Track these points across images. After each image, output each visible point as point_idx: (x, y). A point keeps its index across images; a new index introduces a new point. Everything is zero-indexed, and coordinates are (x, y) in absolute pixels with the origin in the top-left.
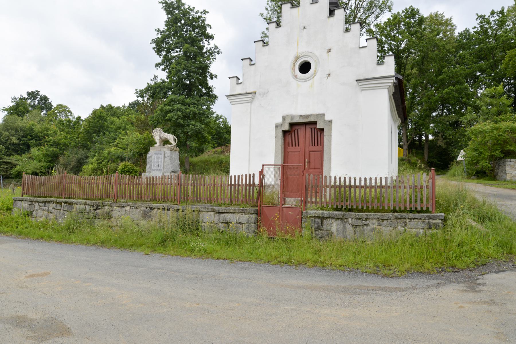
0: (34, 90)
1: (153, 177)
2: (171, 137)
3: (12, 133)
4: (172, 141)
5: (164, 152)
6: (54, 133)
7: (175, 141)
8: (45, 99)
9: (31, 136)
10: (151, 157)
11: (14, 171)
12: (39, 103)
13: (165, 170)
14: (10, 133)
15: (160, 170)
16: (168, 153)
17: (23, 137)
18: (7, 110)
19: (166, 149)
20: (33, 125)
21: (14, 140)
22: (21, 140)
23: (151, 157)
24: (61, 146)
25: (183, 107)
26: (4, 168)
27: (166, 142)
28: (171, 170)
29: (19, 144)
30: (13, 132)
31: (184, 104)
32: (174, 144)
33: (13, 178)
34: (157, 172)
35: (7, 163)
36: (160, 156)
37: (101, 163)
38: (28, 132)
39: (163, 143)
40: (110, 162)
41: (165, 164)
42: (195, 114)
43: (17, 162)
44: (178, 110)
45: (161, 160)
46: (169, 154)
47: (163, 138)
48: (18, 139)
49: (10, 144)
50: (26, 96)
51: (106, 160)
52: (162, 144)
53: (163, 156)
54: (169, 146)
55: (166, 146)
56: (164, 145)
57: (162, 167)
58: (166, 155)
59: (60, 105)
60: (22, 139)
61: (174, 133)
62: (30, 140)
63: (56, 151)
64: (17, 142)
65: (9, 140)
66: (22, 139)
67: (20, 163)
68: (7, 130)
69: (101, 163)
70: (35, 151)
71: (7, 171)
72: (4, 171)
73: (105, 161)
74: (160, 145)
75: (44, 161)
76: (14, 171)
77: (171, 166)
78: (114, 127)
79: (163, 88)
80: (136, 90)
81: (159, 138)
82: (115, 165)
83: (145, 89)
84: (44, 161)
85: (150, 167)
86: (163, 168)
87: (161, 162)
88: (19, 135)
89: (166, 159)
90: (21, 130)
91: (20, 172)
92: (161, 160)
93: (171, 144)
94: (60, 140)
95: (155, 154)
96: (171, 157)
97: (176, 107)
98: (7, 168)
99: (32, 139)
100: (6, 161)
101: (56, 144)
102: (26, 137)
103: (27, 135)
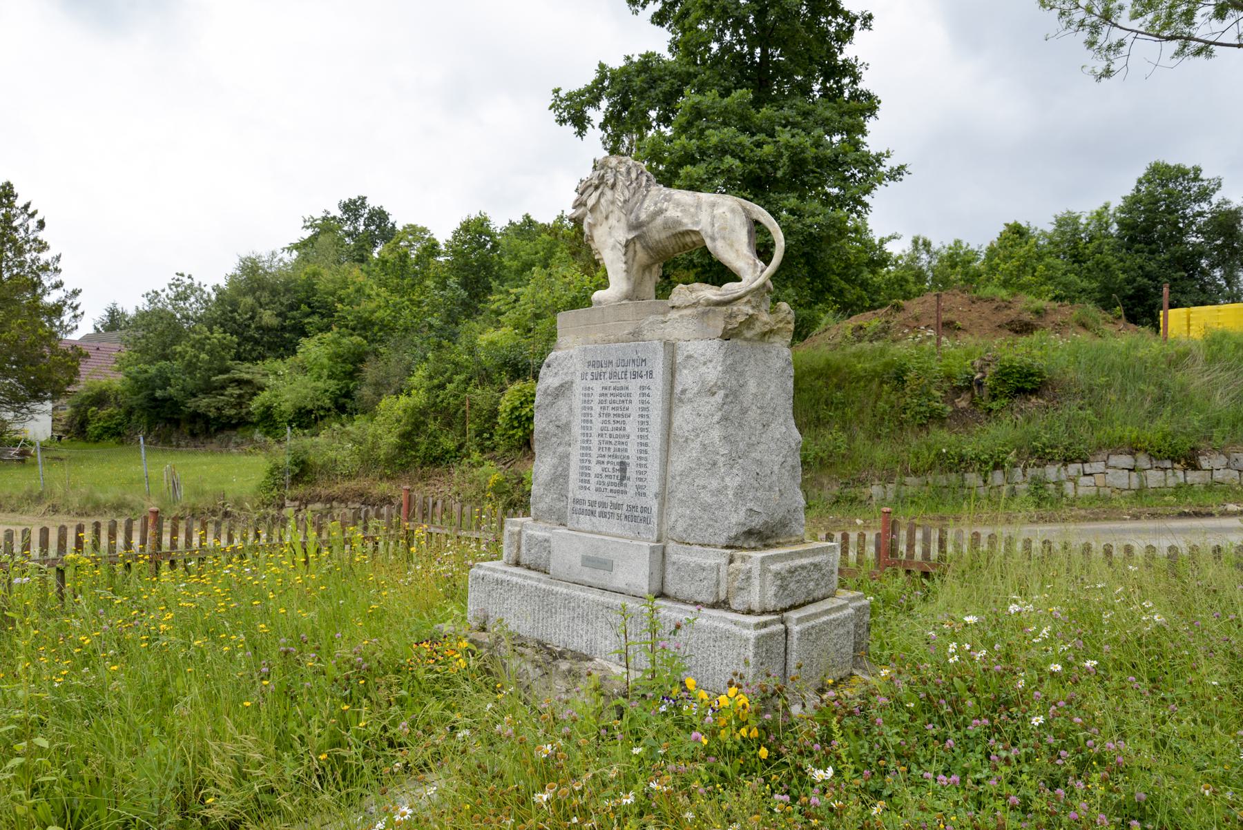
0: (354, 197)
1: (626, 450)
2: (720, 219)
3: (262, 300)
4: (735, 251)
5: (670, 348)
6: (358, 291)
7: (763, 251)
8: (379, 216)
9: (309, 305)
10: (563, 390)
11: (255, 404)
12: (367, 226)
13: (678, 517)
14: (258, 300)
15: (636, 516)
16: (704, 356)
17: (292, 307)
18: (296, 247)
19: (685, 322)
20: (315, 274)
21: (268, 317)
22: (286, 318)
23: (563, 390)
24: (376, 328)
25: (745, 139)
26: (231, 395)
27: (683, 262)
28: (735, 519)
29: (283, 329)
30: (265, 297)
31: (746, 127)
32: (753, 274)
33: (256, 425)
34: (614, 526)
35: (240, 383)
36: (634, 385)
37: (442, 386)
38: (302, 295)
39: (654, 277)
40: (475, 381)
41: (679, 463)
42: (798, 163)
43: (264, 380)
44: (722, 150)
45: (644, 427)
46: (713, 373)
47: (657, 233)
48: (278, 315)
49: (258, 328)
50: (338, 213)
51: (462, 377)
52: (649, 286)
53: (657, 385)
54: (709, 293)
55: (681, 294)
56: (664, 290)
57: (653, 486)
58: (686, 378)
59: (411, 226)
60: (290, 314)
61: (755, 184)
62: (308, 315)
63: (360, 345)
64: (275, 322)
65: (257, 319)
66: (290, 314)
67: (271, 380)
68: (252, 291)
69: (442, 386)
70: (313, 349)
71: (240, 405)
72: (233, 406)
73: (457, 378)
74: (633, 295)
75: (329, 377)
76: (255, 404)
77: (732, 482)
78: (515, 264)
79: (661, 79)
80: (557, 91)
81: (622, 235)
82: (489, 391)
83: (589, 90)
84: (329, 377)
85: (559, 478)
86: (663, 496)
87: (641, 437)
88: (282, 304)
89: (684, 418)
90: (288, 290)
91: (269, 408)
92: (644, 427)
93: (719, 273)
94: (373, 312)
95: (597, 367)
96: (733, 395)
97: (714, 137)
98: (240, 396)
99: (313, 313)
100: (236, 376)
101: (364, 325)
102: (298, 308)
103: (301, 301)
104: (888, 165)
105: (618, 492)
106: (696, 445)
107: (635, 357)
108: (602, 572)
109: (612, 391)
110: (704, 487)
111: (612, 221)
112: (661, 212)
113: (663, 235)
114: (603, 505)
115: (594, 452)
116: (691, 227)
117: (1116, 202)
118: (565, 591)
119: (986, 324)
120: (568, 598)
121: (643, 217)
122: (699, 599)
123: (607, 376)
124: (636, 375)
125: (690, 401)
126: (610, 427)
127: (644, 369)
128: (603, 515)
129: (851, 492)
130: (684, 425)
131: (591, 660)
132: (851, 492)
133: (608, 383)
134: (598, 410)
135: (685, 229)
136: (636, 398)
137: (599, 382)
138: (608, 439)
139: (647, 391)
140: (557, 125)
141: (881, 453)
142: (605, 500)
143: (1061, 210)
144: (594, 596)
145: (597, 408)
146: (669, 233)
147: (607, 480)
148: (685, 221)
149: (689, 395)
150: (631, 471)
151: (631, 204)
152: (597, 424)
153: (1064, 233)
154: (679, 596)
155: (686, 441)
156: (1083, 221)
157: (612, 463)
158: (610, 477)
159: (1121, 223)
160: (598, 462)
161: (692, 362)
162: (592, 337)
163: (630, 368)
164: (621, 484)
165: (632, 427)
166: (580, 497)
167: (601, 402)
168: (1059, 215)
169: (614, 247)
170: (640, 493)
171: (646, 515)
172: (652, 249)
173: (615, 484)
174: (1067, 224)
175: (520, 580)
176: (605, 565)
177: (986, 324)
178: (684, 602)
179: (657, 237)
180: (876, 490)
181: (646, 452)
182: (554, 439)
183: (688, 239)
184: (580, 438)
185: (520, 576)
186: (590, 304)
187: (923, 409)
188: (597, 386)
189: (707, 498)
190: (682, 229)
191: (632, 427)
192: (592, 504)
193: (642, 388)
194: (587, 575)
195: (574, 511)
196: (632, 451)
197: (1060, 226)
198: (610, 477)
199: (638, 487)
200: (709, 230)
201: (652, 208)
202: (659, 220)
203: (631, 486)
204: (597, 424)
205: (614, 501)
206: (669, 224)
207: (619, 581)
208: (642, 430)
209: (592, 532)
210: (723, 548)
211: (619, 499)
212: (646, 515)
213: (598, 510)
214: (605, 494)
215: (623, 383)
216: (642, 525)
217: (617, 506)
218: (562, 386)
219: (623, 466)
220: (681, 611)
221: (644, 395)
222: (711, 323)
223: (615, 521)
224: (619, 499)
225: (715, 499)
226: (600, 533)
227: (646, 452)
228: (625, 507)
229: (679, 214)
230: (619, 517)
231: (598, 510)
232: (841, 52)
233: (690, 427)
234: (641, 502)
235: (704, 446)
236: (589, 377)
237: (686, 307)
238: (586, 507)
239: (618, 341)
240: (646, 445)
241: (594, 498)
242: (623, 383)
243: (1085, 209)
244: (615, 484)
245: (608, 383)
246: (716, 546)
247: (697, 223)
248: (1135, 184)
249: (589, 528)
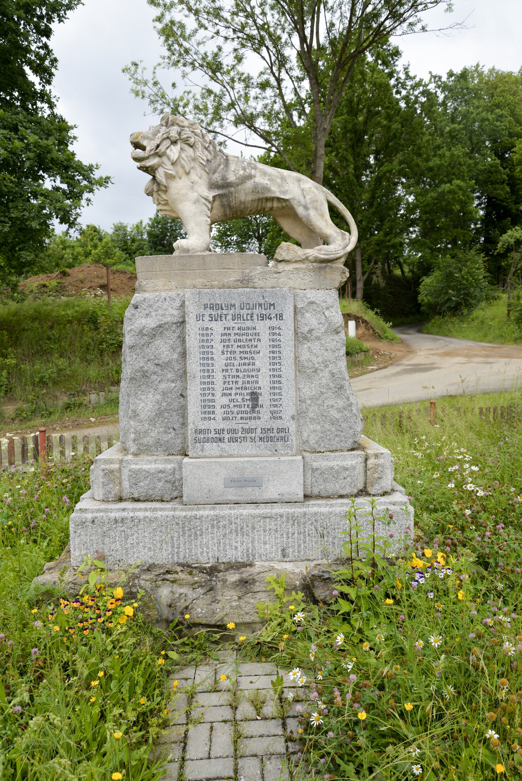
1: (257, 382)
34: (248, 448)
36: (263, 327)
104: (97, 175)
105: (250, 418)
106: (326, 374)
107: (262, 301)
108: (250, 489)
109: (237, 331)
110: (332, 406)
111: (194, 176)
112: (250, 177)
113: (250, 198)
114: (234, 431)
115: (219, 386)
116: (278, 195)
117: (146, 222)
118: (212, 513)
119: (126, 287)
120: (217, 518)
121: (232, 178)
122: (344, 492)
123: (229, 317)
124: (262, 317)
125: (318, 338)
126: (236, 363)
127: (273, 312)
128: (231, 440)
129: (77, 400)
130: (314, 359)
131: (251, 565)
132: (77, 400)
133: (232, 324)
134: (221, 348)
135: (272, 195)
136: (265, 337)
137: (219, 323)
138: (235, 373)
139: (277, 331)
140: (121, 71)
141: (93, 371)
142: (235, 427)
143: (116, 221)
144: (247, 511)
145: (218, 347)
146: (255, 197)
147: (235, 410)
148: (274, 188)
149: (315, 334)
150: (264, 400)
151: (214, 165)
152: (220, 361)
153: (119, 235)
154: (323, 494)
155: (315, 371)
156: (129, 229)
157: (241, 394)
158: (240, 406)
159: (149, 234)
160: (224, 395)
161: (315, 307)
162: (188, 282)
163: (257, 311)
164: (253, 412)
165: (262, 361)
166: (203, 427)
167: (222, 341)
168: (116, 223)
169: (196, 201)
170: (275, 416)
171: (283, 435)
172: (230, 208)
173: (246, 412)
174: (120, 229)
175: (148, 514)
176: (255, 482)
177: (126, 287)
178: (328, 497)
179: (243, 199)
180: (93, 397)
181: (280, 382)
182: (154, 377)
183: (269, 205)
184: (199, 374)
185: (146, 510)
186: (170, 250)
187: (114, 342)
188: (218, 327)
189: (334, 414)
190: (269, 195)
191: (262, 361)
192: (217, 432)
193: (272, 328)
194: (232, 495)
195: (196, 441)
196: (264, 383)
197: (116, 231)
198: (240, 406)
199: (272, 413)
200: (302, 200)
201: (241, 172)
202: (249, 184)
203: (265, 413)
204: (220, 361)
205: (246, 427)
206: (255, 189)
207: (271, 491)
208: (274, 364)
209: (221, 457)
210: (348, 450)
211: (252, 424)
212: (283, 435)
213: (227, 436)
214: (234, 422)
215: (249, 324)
216: (279, 444)
217: (251, 431)
218: (160, 326)
219: (254, 397)
220: (343, 505)
221: (274, 334)
222: (328, 276)
223: (248, 443)
224: (252, 424)
225: (340, 414)
226: (231, 456)
227: (280, 382)
228: (259, 431)
229: (268, 182)
230: (253, 440)
231: (227, 436)
232: (440, 77)
233: (320, 359)
234: (277, 424)
235: (333, 375)
236: (207, 318)
237: (296, 262)
238: (212, 435)
239: (223, 287)
240: (280, 376)
241: (221, 427)
242: (249, 324)
243: (130, 222)
244: (246, 412)
245: (232, 324)
246: (342, 451)
247: (284, 193)
248: (155, 211)
249: (218, 454)
